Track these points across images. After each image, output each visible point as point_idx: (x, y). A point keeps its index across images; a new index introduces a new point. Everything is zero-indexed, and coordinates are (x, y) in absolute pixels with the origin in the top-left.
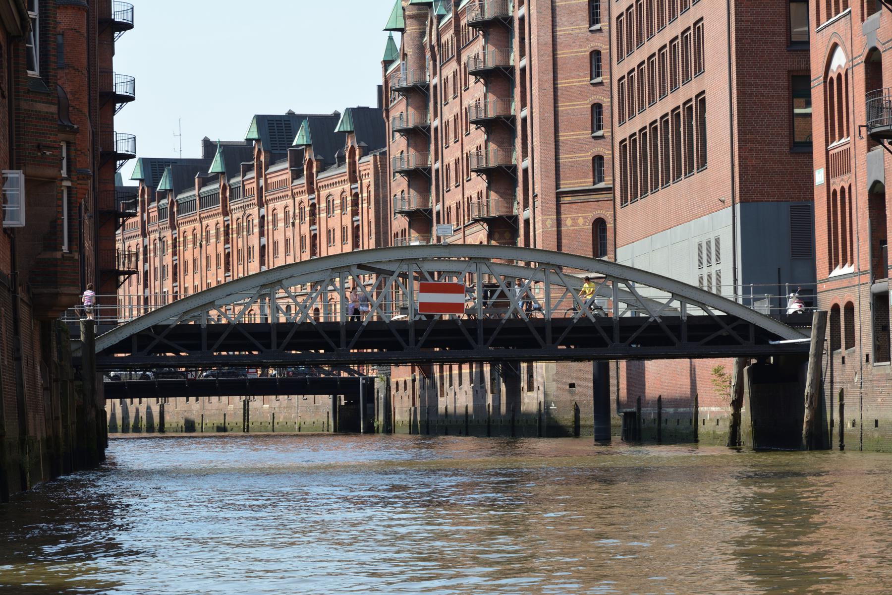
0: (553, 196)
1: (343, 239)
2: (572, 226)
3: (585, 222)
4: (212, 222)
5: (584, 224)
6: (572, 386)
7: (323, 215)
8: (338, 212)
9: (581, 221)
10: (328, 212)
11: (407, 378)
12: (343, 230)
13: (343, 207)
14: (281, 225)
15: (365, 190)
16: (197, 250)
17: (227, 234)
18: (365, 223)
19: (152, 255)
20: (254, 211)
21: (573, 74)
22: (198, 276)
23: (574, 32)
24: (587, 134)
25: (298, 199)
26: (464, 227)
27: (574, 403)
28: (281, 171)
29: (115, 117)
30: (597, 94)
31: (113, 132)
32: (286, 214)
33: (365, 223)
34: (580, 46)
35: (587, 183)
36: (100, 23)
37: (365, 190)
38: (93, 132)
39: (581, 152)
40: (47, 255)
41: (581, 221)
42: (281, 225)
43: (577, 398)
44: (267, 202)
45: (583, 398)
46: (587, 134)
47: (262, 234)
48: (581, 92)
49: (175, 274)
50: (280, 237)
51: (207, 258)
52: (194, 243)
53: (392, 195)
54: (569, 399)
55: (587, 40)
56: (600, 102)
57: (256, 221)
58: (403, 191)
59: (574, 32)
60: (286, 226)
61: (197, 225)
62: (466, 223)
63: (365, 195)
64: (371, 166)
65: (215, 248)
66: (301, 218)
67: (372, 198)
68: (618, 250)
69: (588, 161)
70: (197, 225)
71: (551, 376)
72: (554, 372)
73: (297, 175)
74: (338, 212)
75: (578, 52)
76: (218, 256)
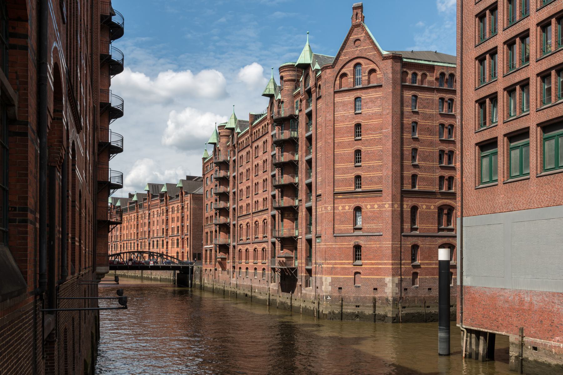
0: (332, 195)
1: (178, 221)
2: (342, 210)
3: (350, 208)
4: (133, 215)
5: (349, 209)
6: (340, 288)
7: (170, 213)
8: (176, 212)
9: (347, 208)
10: (172, 211)
11: (212, 269)
12: (178, 218)
13: (178, 210)
14: (156, 216)
15: (186, 205)
16: (128, 223)
17: (137, 218)
18: (186, 216)
19: (186, 210)
20: (147, 212)
21: (345, 135)
22: (128, 231)
23: (346, 114)
24: (352, 165)
25: (161, 208)
26: (253, 213)
27: (341, 297)
28: (157, 201)
29: (110, 162)
30: (358, 145)
31: (108, 129)
32: (158, 213)
33: (186, 216)
34: (349, 121)
35: (352, 188)
36: (101, 59)
37: (186, 205)
38: (94, 106)
39: (348, 173)
40: (391, 303)
41: (347, 208)
42: (156, 216)
43: (343, 295)
44: (151, 209)
45: (346, 295)
46: (352, 165)
47: (149, 219)
48: (349, 144)
49: (121, 230)
50: (155, 220)
51: (131, 225)
52: (127, 221)
53: (205, 204)
54: (338, 295)
55: (354, 118)
56: (360, 149)
57: (147, 215)
58: (212, 202)
59: (346, 114)
60: (157, 216)
61: (128, 216)
62: (254, 211)
63: (186, 207)
64: (189, 198)
65: (134, 222)
66: (163, 214)
67: (189, 207)
68: (464, 218)
69: (352, 178)
70: (128, 216)
71: (328, 283)
72: (330, 281)
73: (162, 201)
74: (176, 212)
75: (348, 124)
76: (134, 225)
